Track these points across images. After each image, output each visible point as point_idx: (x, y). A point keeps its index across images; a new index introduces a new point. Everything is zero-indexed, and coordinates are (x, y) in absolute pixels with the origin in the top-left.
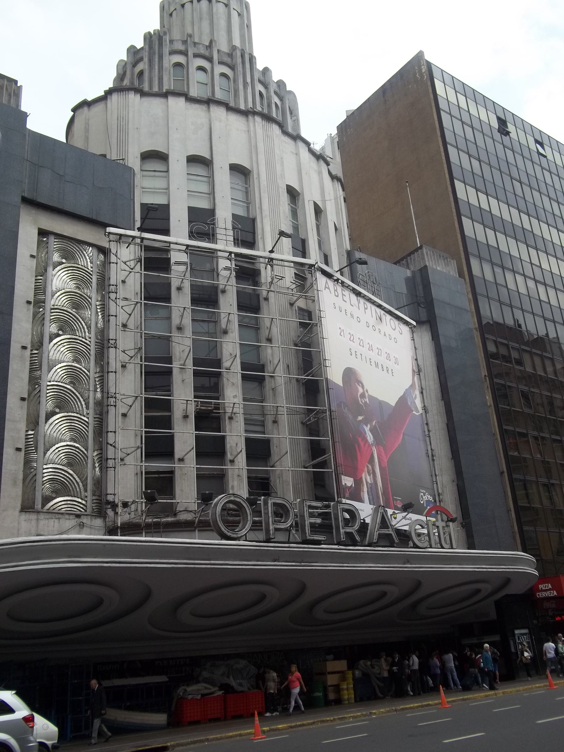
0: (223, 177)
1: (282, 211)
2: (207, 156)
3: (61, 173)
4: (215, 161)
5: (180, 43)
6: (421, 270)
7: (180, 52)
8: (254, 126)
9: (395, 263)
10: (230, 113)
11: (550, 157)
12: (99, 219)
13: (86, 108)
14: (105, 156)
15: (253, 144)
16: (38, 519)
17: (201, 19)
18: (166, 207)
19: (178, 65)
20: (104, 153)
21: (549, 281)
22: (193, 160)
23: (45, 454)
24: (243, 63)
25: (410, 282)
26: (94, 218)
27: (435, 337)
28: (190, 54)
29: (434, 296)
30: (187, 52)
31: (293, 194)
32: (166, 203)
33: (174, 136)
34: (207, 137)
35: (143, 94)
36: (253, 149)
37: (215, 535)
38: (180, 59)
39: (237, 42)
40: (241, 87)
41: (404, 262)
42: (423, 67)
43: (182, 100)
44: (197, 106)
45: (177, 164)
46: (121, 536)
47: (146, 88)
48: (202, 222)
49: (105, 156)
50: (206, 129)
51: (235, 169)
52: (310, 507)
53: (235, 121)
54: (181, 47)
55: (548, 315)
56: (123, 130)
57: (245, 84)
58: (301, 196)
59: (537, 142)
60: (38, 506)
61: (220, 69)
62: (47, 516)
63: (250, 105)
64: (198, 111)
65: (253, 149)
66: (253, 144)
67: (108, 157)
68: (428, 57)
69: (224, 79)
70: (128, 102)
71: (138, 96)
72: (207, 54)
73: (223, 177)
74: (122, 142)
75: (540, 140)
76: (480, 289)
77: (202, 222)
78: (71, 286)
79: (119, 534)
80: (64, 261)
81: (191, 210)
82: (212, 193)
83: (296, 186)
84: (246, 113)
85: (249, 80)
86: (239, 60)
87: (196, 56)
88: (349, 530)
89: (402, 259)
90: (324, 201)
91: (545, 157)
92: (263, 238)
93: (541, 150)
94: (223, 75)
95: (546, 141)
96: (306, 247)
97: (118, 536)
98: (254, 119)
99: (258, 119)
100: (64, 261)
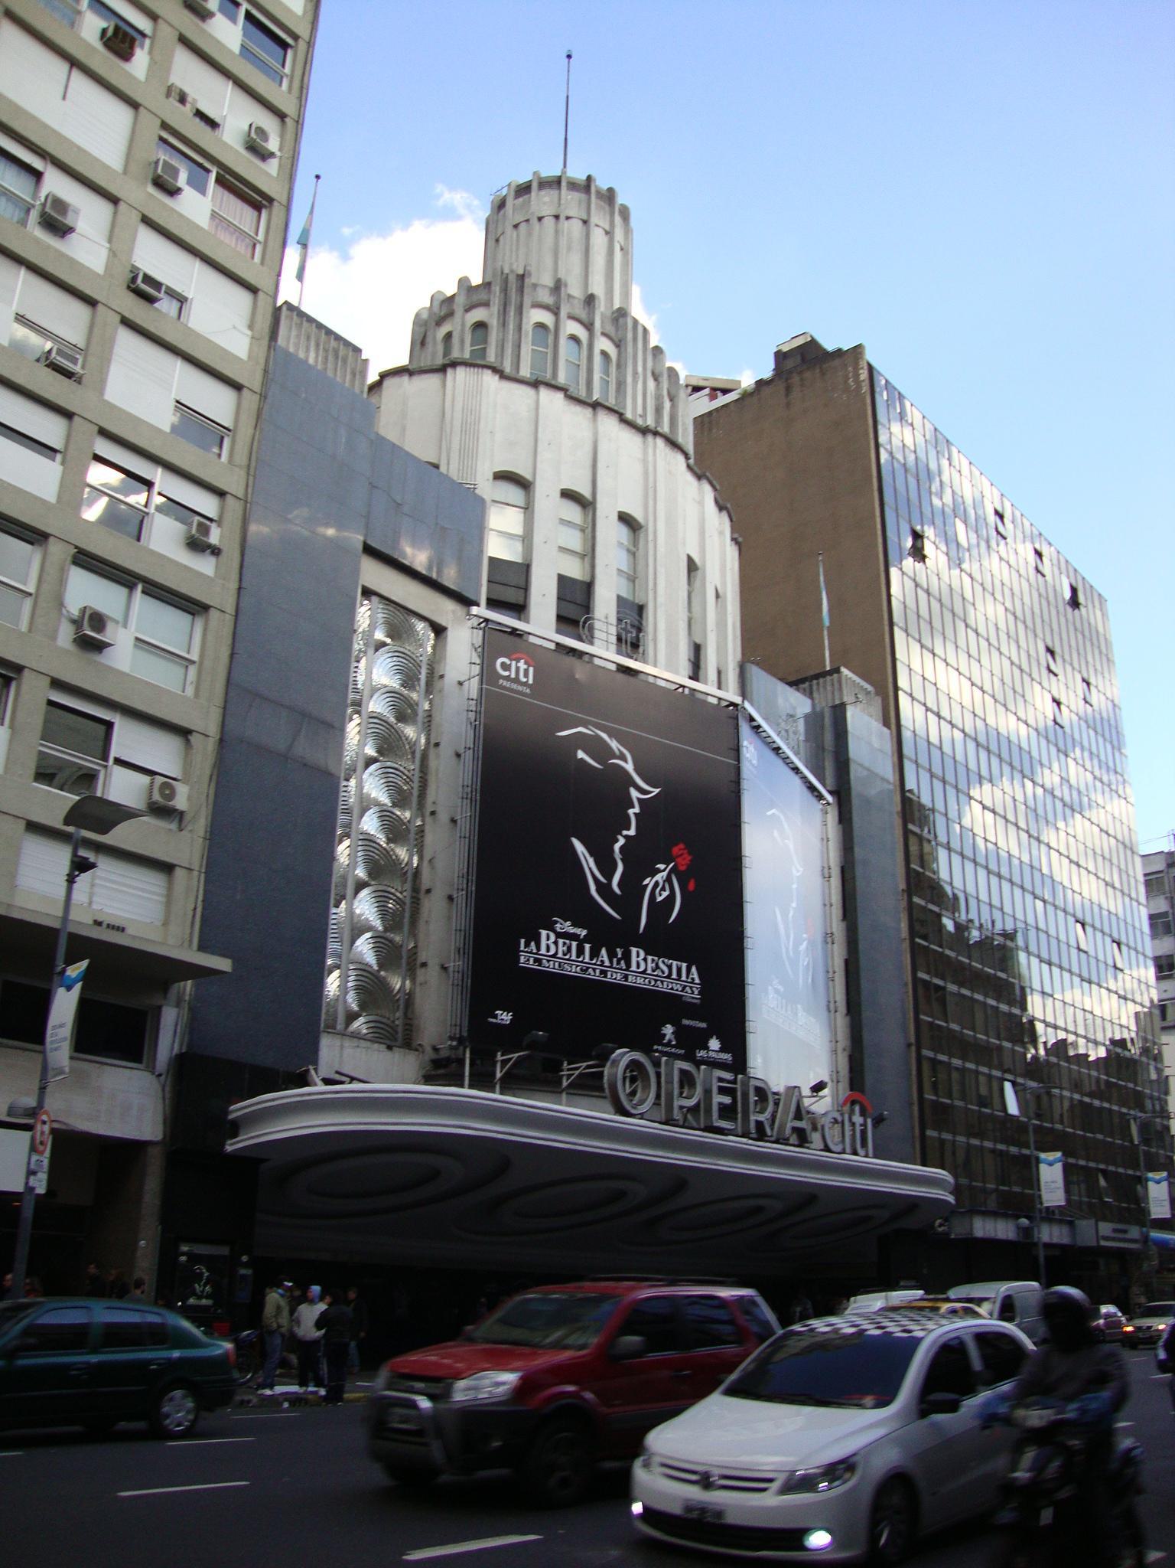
0: (610, 534)
2: (586, 492)
4: (599, 506)
5: (547, 292)
6: (834, 707)
7: (546, 307)
8: (655, 454)
9: (791, 684)
13: (406, 378)
14: (437, 467)
15: (651, 484)
16: (342, 1047)
17: (569, 249)
19: (541, 326)
20: (435, 461)
21: (994, 747)
22: (568, 495)
23: (353, 942)
24: (635, 339)
25: (813, 721)
27: (845, 818)
28: (563, 313)
30: (558, 308)
31: (692, 566)
32: (587, 579)
33: (544, 455)
34: (589, 463)
35: (503, 376)
36: (649, 491)
37: (607, 1104)
38: (547, 318)
39: (597, 288)
40: (629, 379)
41: (807, 685)
43: (560, 395)
44: (578, 409)
46: (471, 1087)
47: (508, 369)
48: (575, 605)
49: (437, 467)
50: (588, 448)
51: (625, 518)
52: (721, 1080)
54: (549, 300)
55: (937, 769)
56: (471, 429)
57: (635, 373)
58: (699, 572)
60: (340, 1026)
62: (355, 1042)
65: (649, 491)
66: (651, 484)
67: (443, 469)
68: (870, 356)
69: (572, 343)
72: (583, 316)
73: (610, 534)
74: (468, 454)
76: (908, 750)
77: (575, 605)
78: (394, 683)
79: (467, 1082)
80: (388, 641)
81: (562, 580)
82: (527, 538)
84: (644, 431)
85: (640, 369)
86: (630, 335)
87: (571, 317)
88: (761, 1118)
89: (803, 681)
90: (724, 583)
92: (655, 640)
93: (1001, 529)
94: (574, 338)
97: (462, 1086)
99: (660, 442)
100: (388, 641)
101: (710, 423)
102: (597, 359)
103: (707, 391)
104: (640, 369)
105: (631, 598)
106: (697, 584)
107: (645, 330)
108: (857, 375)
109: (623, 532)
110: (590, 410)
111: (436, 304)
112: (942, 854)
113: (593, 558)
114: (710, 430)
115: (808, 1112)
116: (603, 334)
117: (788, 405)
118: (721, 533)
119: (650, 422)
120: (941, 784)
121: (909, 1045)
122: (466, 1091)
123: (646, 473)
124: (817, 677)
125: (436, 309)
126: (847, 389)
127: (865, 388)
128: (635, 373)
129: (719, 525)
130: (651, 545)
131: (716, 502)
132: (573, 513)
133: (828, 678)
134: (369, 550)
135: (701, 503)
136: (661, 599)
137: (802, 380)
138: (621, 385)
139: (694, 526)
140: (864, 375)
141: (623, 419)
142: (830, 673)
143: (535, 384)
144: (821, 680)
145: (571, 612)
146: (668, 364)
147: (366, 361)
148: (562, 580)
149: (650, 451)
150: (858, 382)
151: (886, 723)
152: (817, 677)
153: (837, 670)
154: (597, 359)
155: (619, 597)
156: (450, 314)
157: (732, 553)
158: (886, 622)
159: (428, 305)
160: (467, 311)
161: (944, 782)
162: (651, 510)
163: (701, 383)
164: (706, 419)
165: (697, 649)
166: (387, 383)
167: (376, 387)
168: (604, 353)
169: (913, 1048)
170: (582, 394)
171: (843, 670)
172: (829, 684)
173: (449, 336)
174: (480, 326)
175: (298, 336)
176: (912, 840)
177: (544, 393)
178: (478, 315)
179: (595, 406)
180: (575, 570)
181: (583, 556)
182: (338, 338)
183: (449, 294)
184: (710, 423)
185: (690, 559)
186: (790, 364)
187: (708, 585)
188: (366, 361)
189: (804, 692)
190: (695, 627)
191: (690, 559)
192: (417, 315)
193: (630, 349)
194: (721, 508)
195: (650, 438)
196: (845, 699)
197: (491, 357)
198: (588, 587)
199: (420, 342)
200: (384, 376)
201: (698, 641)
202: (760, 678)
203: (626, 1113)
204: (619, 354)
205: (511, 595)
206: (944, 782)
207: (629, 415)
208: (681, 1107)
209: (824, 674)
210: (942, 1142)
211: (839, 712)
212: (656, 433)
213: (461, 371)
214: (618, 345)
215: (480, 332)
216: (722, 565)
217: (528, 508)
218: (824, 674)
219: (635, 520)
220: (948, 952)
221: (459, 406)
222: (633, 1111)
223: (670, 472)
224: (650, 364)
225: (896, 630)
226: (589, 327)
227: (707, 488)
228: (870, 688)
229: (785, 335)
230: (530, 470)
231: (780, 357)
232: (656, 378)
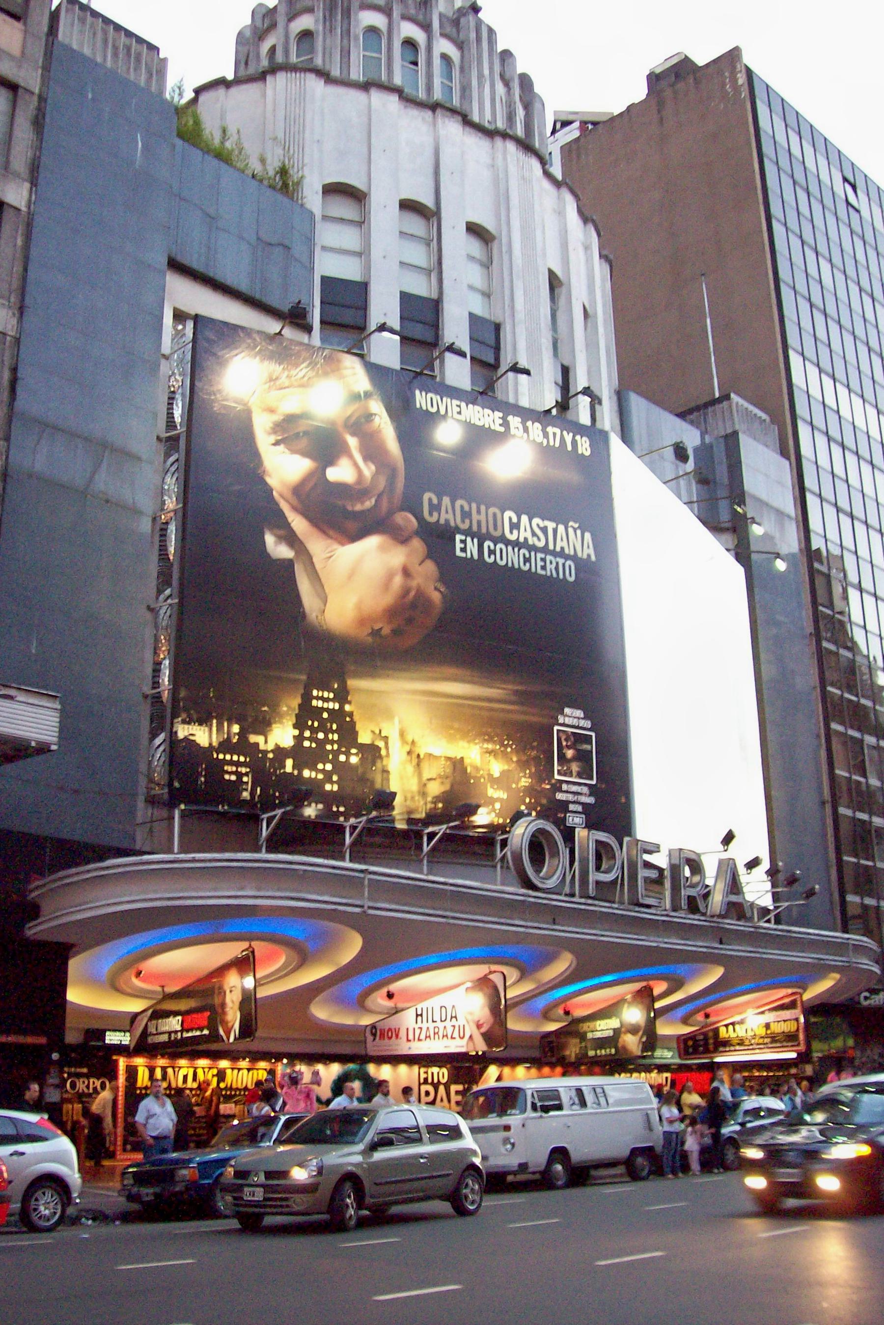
0: (457, 244)
1: (542, 315)
2: (428, 201)
3: (212, 211)
6: (726, 437)
8: (505, 159)
10: (468, 129)
11: (865, 213)
12: (264, 300)
13: (221, 91)
18: (363, 288)
19: (372, 30)
22: (408, 206)
24: (479, 39)
26: (258, 296)
28: (396, 14)
29: (746, 488)
30: (391, 9)
31: (554, 282)
32: (434, 296)
33: (380, 162)
34: (430, 170)
40: (474, 83)
42: (739, 75)
43: (394, 98)
45: (384, 214)
47: (336, 72)
50: (429, 153)
51: (474, 230)
53: (476, 147)
57: (481, 76)
58: (564, 290)
59: (845, 180)
61: (443, 46)
63: (488, 116)
64: (358, 96)
68: (748, 59)
70: (305, 90)
71: (322, 82)
73: (457, 244)
75: (852, 180)
76: (810, 482)
81: (405, 298)
82: (363, 254)
83: (559, 272)
84: (490, 133)
85: (486, 72)
86: (473, 35)
87: (405, 17)
89: (690, 411)
90: (593, 301)
91: (858, 211)
95: (860, 184)
96: (571, 381)
98: (506, 147)
99: (511, 146)
101: (578, 148)
102: (437, 61)
103: (576, 125)
104: (486, 72)
105: (486, 316)
106: (562, 302)
107: (491, 31)
108: (734, 80)
109: (475, 247)
110: (429, 113)
111: (259, 17)
112: (853, 594)
113: (440, 273)
114: (578, 157)
115: (30, 476)
116: (443, 35)
117: (661, 120)
118: (587, 248)
119: (501, 124)
120: (849, 520)
121: (823, 803)
122: (264, 855)
123: (496, 181)
124: (706, 405)
125: (259, 23)
126: (724, 96)
127: (745, 94)
128: (481, 76)
129: (580, 235)
130: (505, 257)
131: (580, 212)
132: (415, 225)
133: (718, 407)
134: (176, 266)
135: (561, 213)
136: (520, 316)
137: (675, 93)
138: (465, 89)
139: (555, 235)
140: (742, 79)
141: (466, 121)
142: (719, 401)
143: (365, 86)
144: (710, 409)
145: (419, 331)
146: (519, 71)
147: (165, 60)
148: (405, 298)
149: (500, 156)
150: (736, 88)
151: (784, 453)
152: (706, 405)
153: (727, 397)
154: (437, 61)
155: (471, 315)
156: (273, 26)
157: (600, 270)
158: (779, 345)
159: (249, 21)
160: (290, 20)
161: (852, 517)
162: (503, 218)
163: (570, 118)
164: (574, 147)
165: (566, 372)
166: (202, 98)
167: (195, 101)
168: (445, 57)
169: (828, 808)
170: (422, 95)
171: (732, 395)
172: (719, 415)
173: (273, 49)
174: (306, 35)
175: (81, 32)
176: (819, 582)
177: (377, 98)
178: (305, 22)
179: (434, 107)
180: (420, 287)
181: (428, 272)
182: (129, 34)
183: (271, 6)
184: (578, 148)
185: (551, 272)
186: (664, 84)
187: (574, 301)
188: (165, 60)
189: (692, 423)
190: (563, 348)
191: (551, 272)
192: (240, 34)
193: (474, 50)
194: (585, 218)
195: (499, 141)
196: (737, 427)
197: (319, 61)
198: (436, 305)
199: (242, 60)
200: (198, 91)
201: (566, 363)
202: (637, 404)
203: (534, 888)
204: (462, 57)
205: (348, 316)
206: (852, 517)
207: (476, 118)
208: (598, 883)
209: (714, 402)
210: (865, 907)
211: (731, 441)
212: (505, 136)
213: (281, 77)
214: (460, 46)
215: (305, 45)
216: (590, 281)
217: (362, 223)
218: (714, 402)
219: (487, 231)
220: (863, 701)
221: (281, 114)
222: (540, 885)
223: (523, 178)
224: (497, 68)
225: (791, 353)
226: (426, 27)
227: (569, 198)
228: (764, 416)
229: (657, 58)
230: (365, 179)
231: (654, 79)
232: (507, 84)
